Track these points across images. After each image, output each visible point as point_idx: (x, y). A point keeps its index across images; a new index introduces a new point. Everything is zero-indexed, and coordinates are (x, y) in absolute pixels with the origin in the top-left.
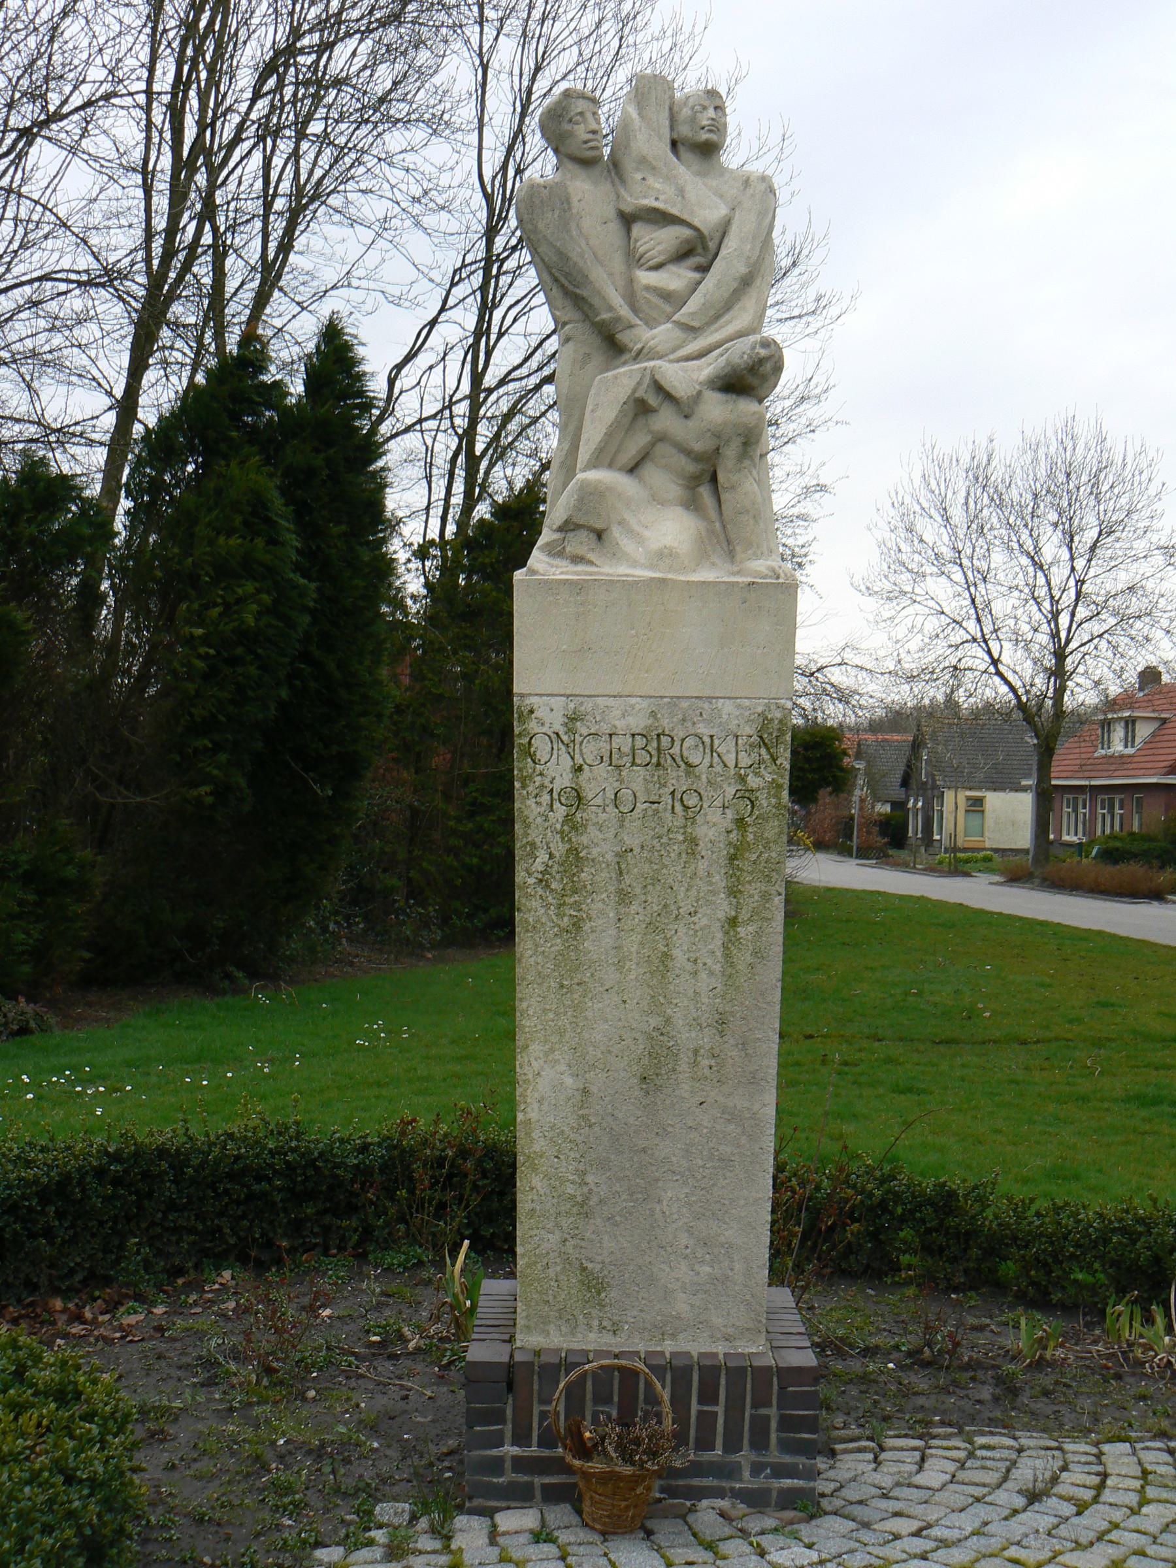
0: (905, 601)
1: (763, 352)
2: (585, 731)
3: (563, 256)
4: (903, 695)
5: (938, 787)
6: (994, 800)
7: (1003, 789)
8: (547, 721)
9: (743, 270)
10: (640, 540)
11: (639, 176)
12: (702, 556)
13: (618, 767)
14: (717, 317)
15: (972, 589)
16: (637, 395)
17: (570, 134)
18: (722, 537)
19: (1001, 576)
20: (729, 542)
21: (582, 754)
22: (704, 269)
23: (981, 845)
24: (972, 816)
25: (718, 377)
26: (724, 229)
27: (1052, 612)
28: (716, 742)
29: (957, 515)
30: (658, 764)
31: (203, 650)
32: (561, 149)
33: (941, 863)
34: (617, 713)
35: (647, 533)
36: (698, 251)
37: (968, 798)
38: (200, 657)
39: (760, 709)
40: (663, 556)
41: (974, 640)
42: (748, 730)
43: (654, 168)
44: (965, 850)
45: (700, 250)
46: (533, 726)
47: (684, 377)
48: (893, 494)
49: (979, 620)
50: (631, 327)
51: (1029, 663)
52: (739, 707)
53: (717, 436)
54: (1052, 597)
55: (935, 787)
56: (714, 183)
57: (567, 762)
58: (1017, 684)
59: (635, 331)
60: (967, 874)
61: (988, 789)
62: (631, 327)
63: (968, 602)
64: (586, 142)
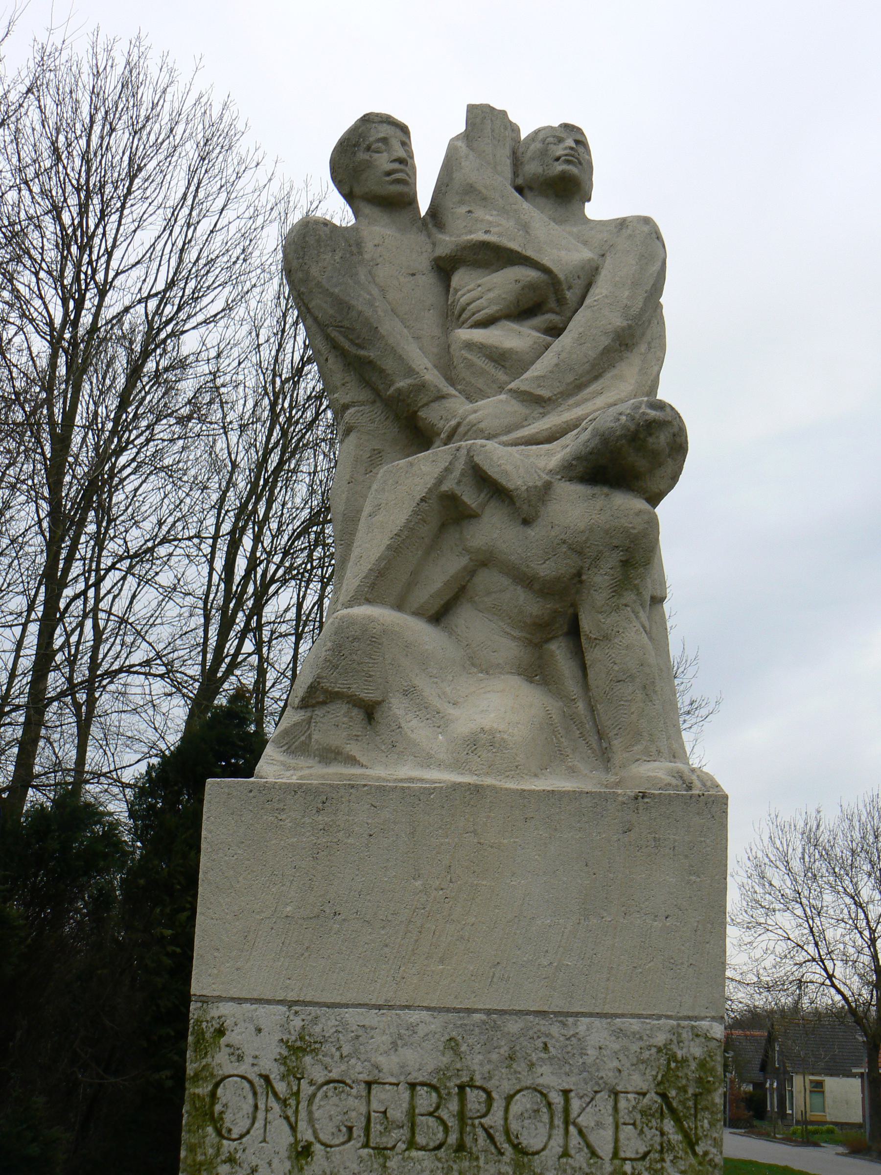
0: (760, 930)
1: (653, 413)
2: (320, 1076)
3: (343, 306)
4: (761, 1001)
5: (788, 1072)
6: (831, 1084)
7: (837, 1075)
8: (249, 1051)
9: (618, 321)
10: (438, 720)
11: (463, 209)
12: (552, 755)
13: (380, 1150)
14: (579, 387)
15: (811, 922)
16: (444, 488)
17: (368, 165)
18: (588, 726)
19: (831, 912)
20: (601, 735)
21: (311, 1120)
22: (555, 331)
23: (823, 1119)
24: (814, 1095)
25: (578, 458)
26: (589, 277)
27: (870, 939)
28: (576, 1104)
29: (796, 865)
30: (460, 1147)
31: (170, 949)
32: (357, 190)
33: (794, 1133)
34: (382, 1040)
35: (452, 711)
36: (546, 302)
37: (811, 1081)
38: (168, 954)
39: (660, 1039)
40: (477, 744)
41: (814, 960)
42: (638, 1081)
43: (485, 199)
44: (812, 1123)
45: (552, 304)
46: (222, 1061)
47: (519, 464)
48: (749, 851)
49: (816, 944)
50: (441, 397)
51: (856, 977)
52: (619, 1033)
53: (578, 550)
54: (870, 928)
55: (786, 1072)
56: (575, 230)
57: (281, 1136)
58: (848, 993)
59: (448, 403)
60: (816, 1145)
61: (827, 1075)
62: (441, 397)
63: (807, 931)
64: (389, 174)
